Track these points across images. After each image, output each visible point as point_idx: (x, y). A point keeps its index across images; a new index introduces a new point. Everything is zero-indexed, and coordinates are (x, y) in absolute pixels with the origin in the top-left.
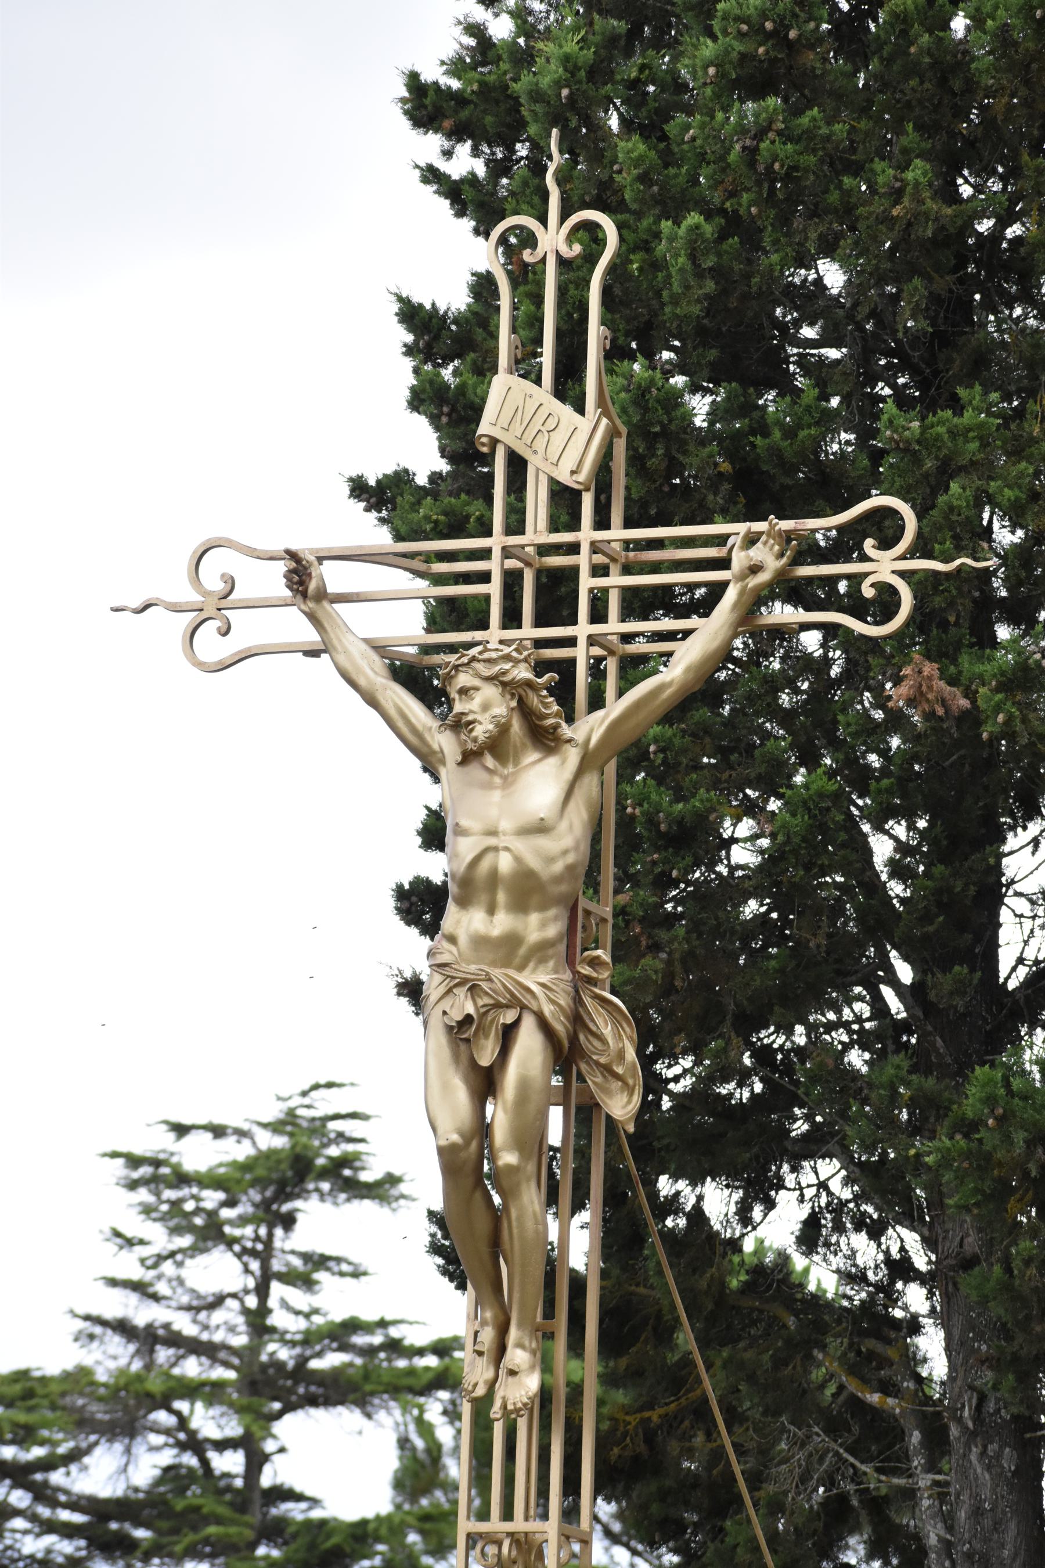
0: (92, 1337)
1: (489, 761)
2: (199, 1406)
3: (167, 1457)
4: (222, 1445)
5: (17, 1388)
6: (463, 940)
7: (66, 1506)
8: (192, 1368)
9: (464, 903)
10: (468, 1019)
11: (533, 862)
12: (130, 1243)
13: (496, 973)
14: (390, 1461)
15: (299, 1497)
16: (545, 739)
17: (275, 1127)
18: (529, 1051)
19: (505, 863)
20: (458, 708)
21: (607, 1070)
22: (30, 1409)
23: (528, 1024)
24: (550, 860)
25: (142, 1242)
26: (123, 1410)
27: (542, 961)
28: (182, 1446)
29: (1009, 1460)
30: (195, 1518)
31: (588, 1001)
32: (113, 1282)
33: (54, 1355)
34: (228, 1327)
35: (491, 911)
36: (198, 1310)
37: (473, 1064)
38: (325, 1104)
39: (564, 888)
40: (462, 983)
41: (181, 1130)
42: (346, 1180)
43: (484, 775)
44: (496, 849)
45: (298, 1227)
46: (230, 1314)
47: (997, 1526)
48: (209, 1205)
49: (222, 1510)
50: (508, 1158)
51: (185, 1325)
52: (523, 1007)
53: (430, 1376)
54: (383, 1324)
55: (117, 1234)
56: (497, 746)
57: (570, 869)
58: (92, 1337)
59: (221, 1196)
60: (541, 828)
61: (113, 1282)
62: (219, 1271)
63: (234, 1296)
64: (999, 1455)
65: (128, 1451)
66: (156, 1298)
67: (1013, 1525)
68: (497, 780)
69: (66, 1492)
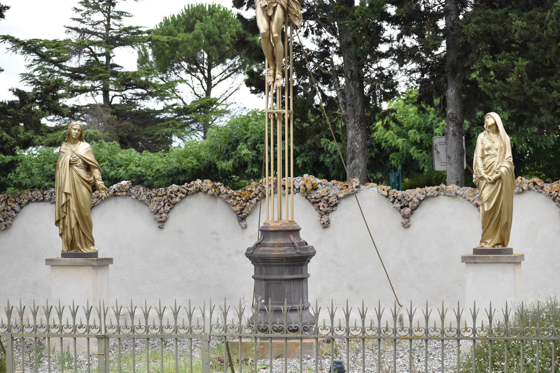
0: (69, 32)
2: (96, 47)
3: (88, 58)
4: (100, 55)
7: (67, 70)
8: (93, 38)
10: (266, 6)
12: (79, 10)
15: (118, 66)
18: (279, 12)
21: (295, 15)
22: (59, 49)
23: (279, 6)
25: (81, 10)
26: (79, 48)
28: (91, 56)
29: (358, 85)
30: (97, 72)
32: (74, 19)
33: (61, 36)
34: (101, 29)
46: (101, 25)
47: (356, 98)
49: (103, 70)
51: (91, 29)
52: (278, 3)
54: (137, 27)
55: (76, 9)
58: (69, 32)
61: (74, 19)
62: (98, 16)
63: (102, 22)
64: (356, 84)
67: (359, 99)
69: (67, 67)
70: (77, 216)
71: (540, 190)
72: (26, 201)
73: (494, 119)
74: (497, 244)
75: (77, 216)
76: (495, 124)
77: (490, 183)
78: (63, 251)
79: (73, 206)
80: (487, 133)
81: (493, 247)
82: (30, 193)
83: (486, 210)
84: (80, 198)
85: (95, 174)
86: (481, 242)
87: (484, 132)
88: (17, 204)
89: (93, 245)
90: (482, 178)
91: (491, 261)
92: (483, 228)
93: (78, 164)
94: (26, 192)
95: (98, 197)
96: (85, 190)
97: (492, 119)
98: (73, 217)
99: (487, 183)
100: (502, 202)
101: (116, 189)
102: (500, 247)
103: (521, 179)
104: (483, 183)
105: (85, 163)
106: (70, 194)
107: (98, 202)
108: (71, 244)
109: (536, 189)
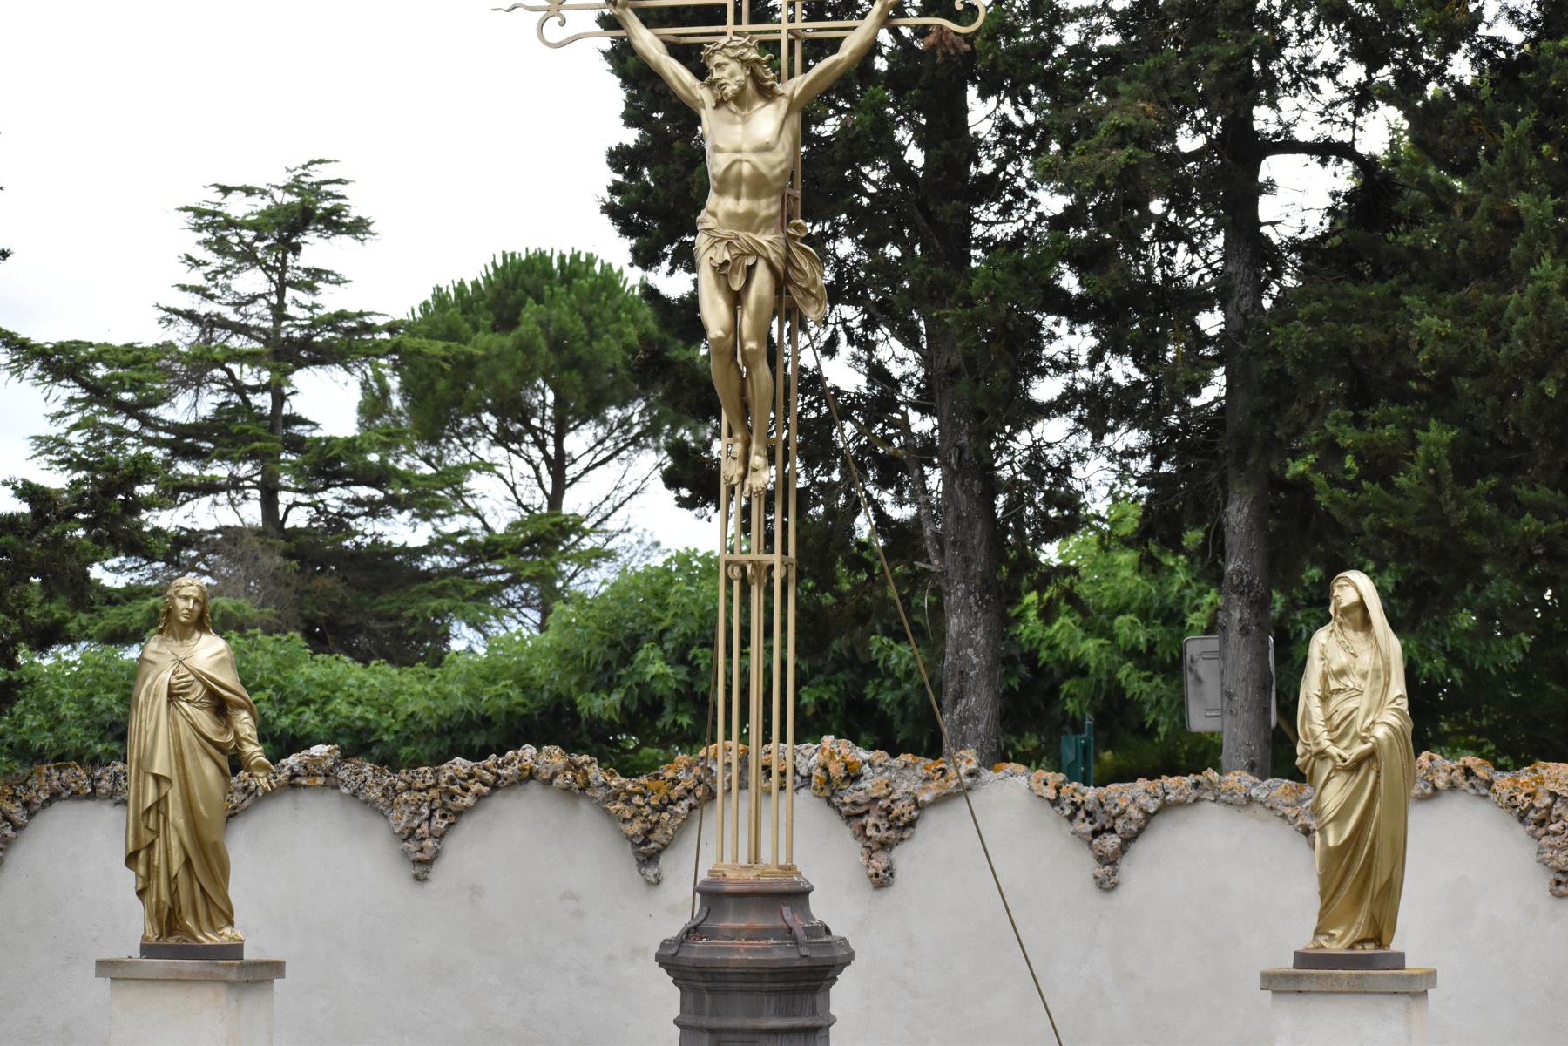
0: (170, 321)
1: (733, 107)
2: (246, 367)
4: (255, 390)
5: (130, 356)
6: (720, 214)
7: (162, 429)
8: (237, 342)
9: (721, 192)
10: (726, 262)
11: (764, 169)
12: (198, 264)
13: (741, 234)
14: (355, 396)
15: (305, 422)
16: (767, 94)
17: (287, 189)
19: (746, 169)
20: (716, 75)
21: (806, 291)
22: (141, 370)
23: (761, 265)
24: (773, 167)
25: (205, 263)
26: (198, 366)
27: (768, 227)
29: (977, 488)
30: (244, 437)
31: (794, 250)
32: (184, 288)
33: (149, 334)
34: (259, 315)
35: (738, 198)
36: (240, 305)
37: (729, 288)
38: (318, 174)
39: (780, 184)
40: (721, 240)
41: (226, 190)
42: (334, 223)
43: (730, 115)
44: (741, 161)
45: (303, 252)
46: (260, 307)
48: (248, 240)
49: (262, 432)
50: (751, 345)
51: (230, 315)
52: (759, 255)
53: (389, 346)
54: (361, 314)
55: (190, 258)
56: (740, 99)
57: (784, 172)
58: (170, 321)
59: (254, 233)
60: (766, 148)
61: (184, 288)
62: (253, 281)
63: (262, 296)
64: (971, 485)
65: (197, 392)
66: (212, 297)
67: (979, 526)
68: (738, 119)
70: (186, 840)
71: (1484, 791)
72: (44, 796)
73: (1356, 588)
74: (1362, 941)
75: (186, 840)
76: (1361, 605)
77: (1345, 769)
78: (144, 938)
79: (176, 814)
80: (1337, 628)
81: (1351, 947)
82: (56, 775)
83: (1331, 843)
84: (196, 791)
85: (239, 726)
86: (1317, 933)
87: (1329, 627)
88: (18, 803)
89: (231, 923)
90: (1322, 755)
91: (1344, 988)
92: (1322, 894)
93: (192, 697)
94: (45, 771)
95: (245, 789)
96: (209, 770)
97: (1351, 589)
98: (174, 843)
99: (1335, 769)
100: (1377, 824)
101: (296, 769)
102: (1370, 949)
103: (1431, 759)
104: (1325, 769)
105: (212, 693)
106: (169, 780)
107: (246, 804)
108: (168, 920)
109: (1473, 786)
